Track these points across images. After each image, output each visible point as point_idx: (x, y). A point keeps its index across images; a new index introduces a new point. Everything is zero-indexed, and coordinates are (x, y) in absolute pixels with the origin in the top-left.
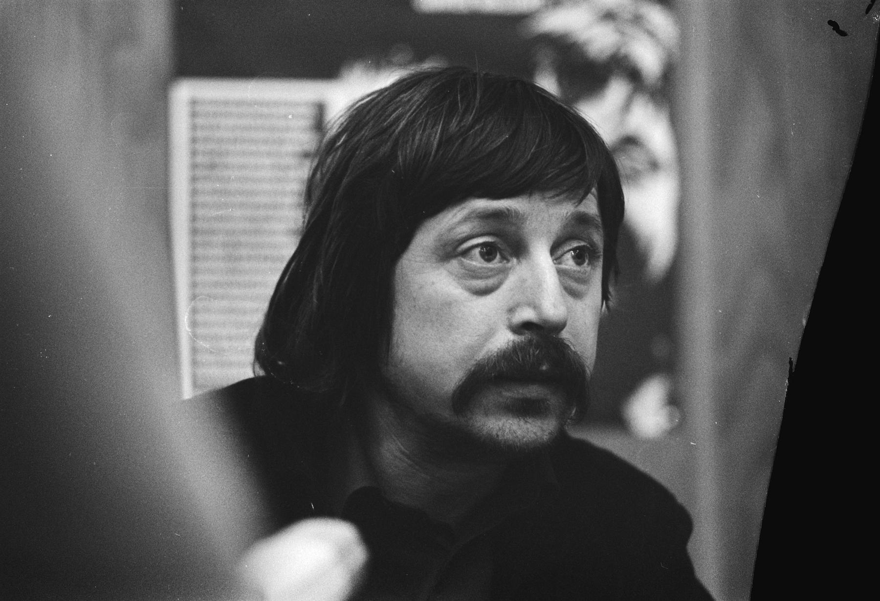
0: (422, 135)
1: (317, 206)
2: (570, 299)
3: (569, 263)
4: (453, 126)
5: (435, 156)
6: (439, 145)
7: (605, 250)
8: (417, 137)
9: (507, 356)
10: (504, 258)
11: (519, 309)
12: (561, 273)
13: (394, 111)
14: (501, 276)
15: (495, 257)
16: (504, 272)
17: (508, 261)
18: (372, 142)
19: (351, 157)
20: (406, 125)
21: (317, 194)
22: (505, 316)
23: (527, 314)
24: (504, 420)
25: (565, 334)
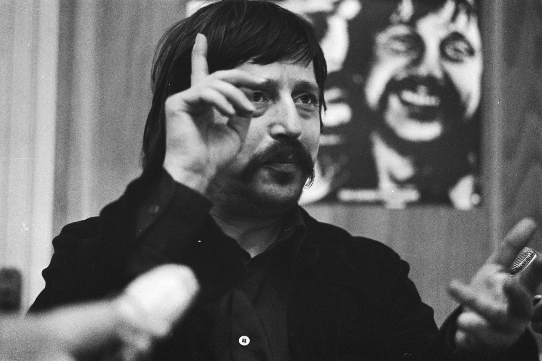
0: (215, 33)
1: (158, 81)
2: (303, 120)
3: (300, 102)
4: (233, 25)
5: (224, 40)
6: (225, 35)
7: (312, 166)
8: (213, 32)
9: (272, 150)
10: (265, 99)
11: (275, 126)
12: (297, 107)
13: (197, 23)
14: (263, 109)
15: (259, 99)
16: (267, 107)
17: (268, 101)
18: (187, 38)
19: (176, 48)
20: (206, 26)
21: (157, 76)
22: (267, 129)
23: (279, 129)
24: (272, 185)
25: (300, 138)
